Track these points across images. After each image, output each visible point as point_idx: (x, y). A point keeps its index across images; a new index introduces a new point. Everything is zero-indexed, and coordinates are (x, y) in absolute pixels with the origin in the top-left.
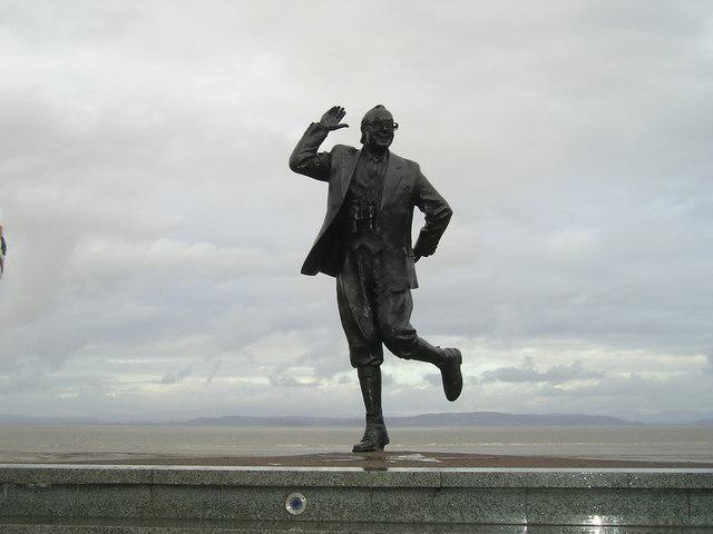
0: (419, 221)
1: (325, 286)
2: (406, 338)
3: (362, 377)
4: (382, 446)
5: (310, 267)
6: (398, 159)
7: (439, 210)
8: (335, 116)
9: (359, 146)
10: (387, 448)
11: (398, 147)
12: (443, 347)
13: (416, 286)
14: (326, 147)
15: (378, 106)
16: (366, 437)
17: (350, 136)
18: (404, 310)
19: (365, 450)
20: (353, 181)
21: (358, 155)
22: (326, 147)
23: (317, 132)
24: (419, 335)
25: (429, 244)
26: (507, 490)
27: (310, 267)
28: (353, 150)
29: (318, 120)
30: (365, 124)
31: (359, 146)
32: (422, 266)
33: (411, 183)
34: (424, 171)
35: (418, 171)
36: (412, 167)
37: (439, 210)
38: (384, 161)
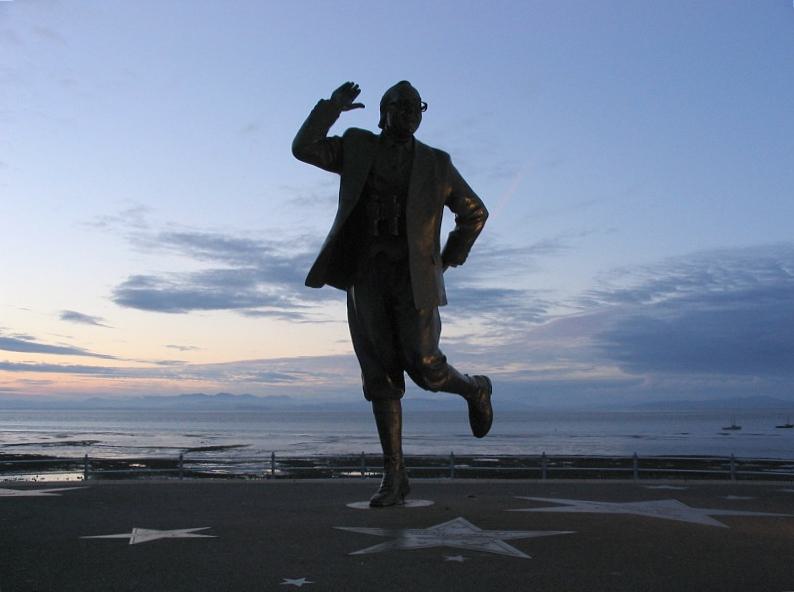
3: (377, 412)
6: (425, 148)
9: (378, 131)
11: (426, 133)
14: (337, 130)
17: (366, 118)
22: (337, 130)
28: (367, 135)
29: (328, 96)
30: (387, 104)
31: (378, 131)
36: (441, 158)
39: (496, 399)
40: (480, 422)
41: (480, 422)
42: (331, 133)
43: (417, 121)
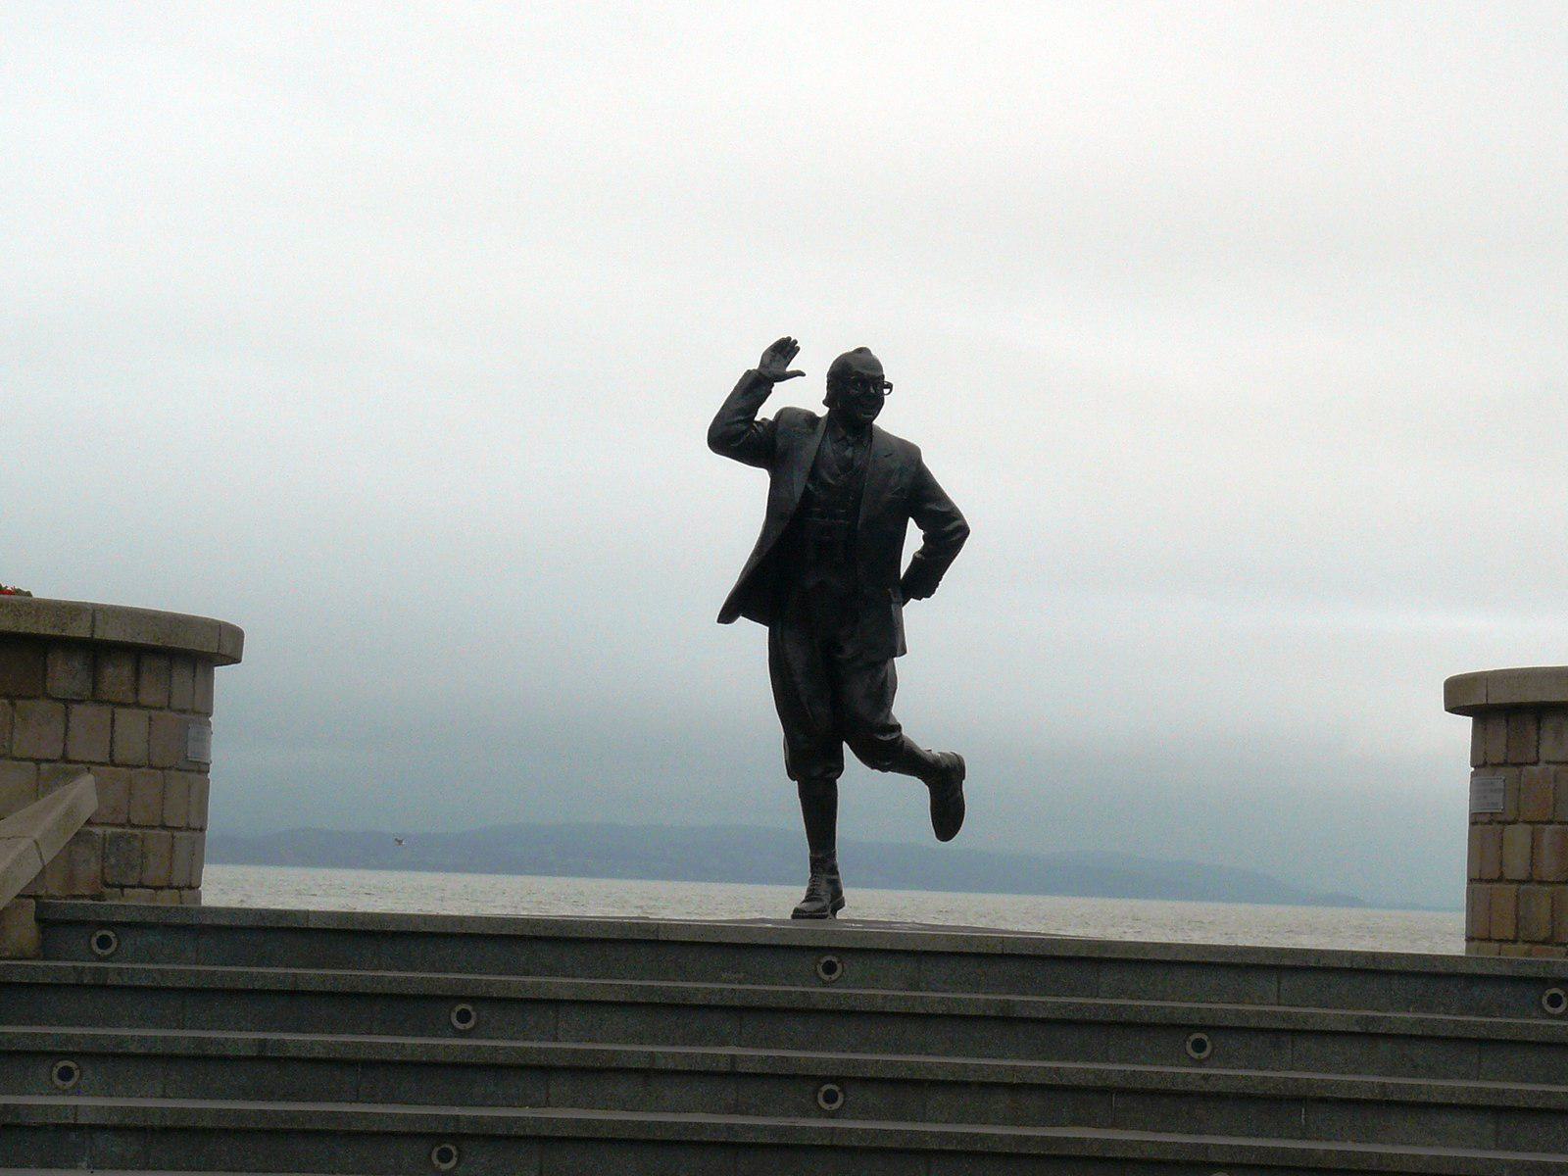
0: (914, 539)
1: (753, 636)
2: (888, 738)
4: (834, 912)
5: (727, 615)
7: (951, 527)
8: (785, 349)
9: (822, 411)
10: (840, 915)
11: (891, 420)
12: (935, 752)
13: (904, 652)
14: (767, 412)
15: (860, 350)
16: (811, 897)
18: (883, 691)
19: (811, 916)
20: (813, 475)
21: (821, 427)
22: (767, 412)
23: (756, 386)
24: (904, 732)
25: (925, 578)
26: (1220, 1097)
27: (727, 615)
28: (812, 419)
29: (755, 365)
31: (822, 411)
32: (914, 614)
33: (906, 480)
34: (928, 461)
35: (919, 461)
36: (909, 455)
37: (951, 527)
38: (865, 442)
39: (969, 788)
40: (948, 816)
41: (948, 816)
42: (911, 520)
43: (877, 403)
